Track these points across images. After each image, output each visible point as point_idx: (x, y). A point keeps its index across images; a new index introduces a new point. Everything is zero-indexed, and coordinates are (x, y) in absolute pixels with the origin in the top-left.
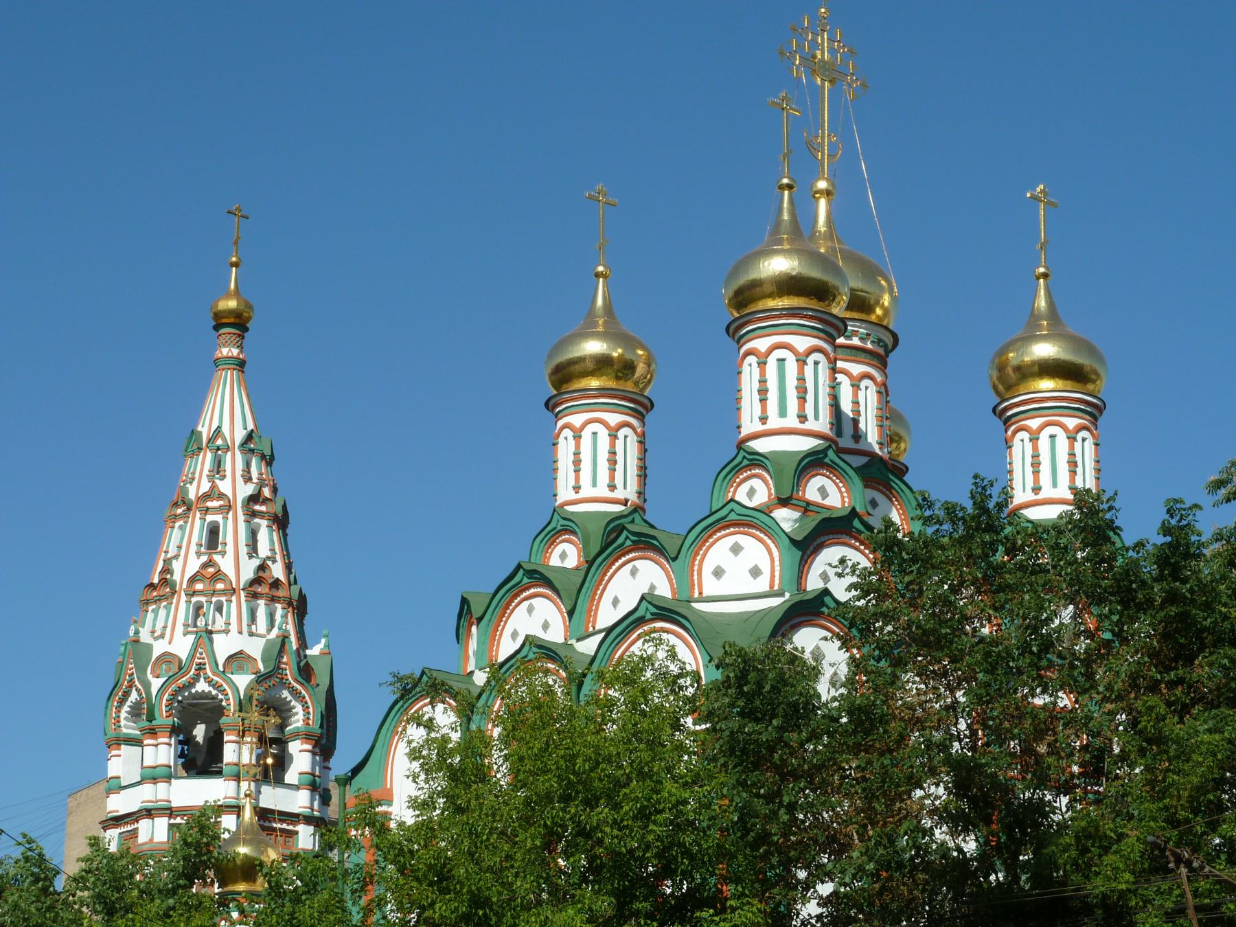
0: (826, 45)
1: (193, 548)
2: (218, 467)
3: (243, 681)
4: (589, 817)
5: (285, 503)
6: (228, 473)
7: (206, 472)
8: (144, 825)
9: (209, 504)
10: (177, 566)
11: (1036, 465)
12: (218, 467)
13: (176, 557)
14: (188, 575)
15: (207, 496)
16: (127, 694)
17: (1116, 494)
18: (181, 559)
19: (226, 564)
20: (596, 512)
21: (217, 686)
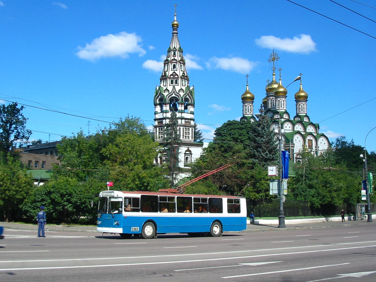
0: (198, 269)
1: (170, 69)
2: (174, 54)
3: (182, 94)
4: (330, 177)
5: (352, 140)
6: (177, 55)
7: (172, 55)
8: (164, 121)
9: (173, 61)
10: (167, 73)
11: (304, 108)
12: (174, 54)
13: (167, 71)
14: (170, 75)
15: (173, 60)
16: (158, 96)
17: (152, 125)
18: (168, 71)
19: (177, 72)
20: (278, 187)
21: (177, 95)
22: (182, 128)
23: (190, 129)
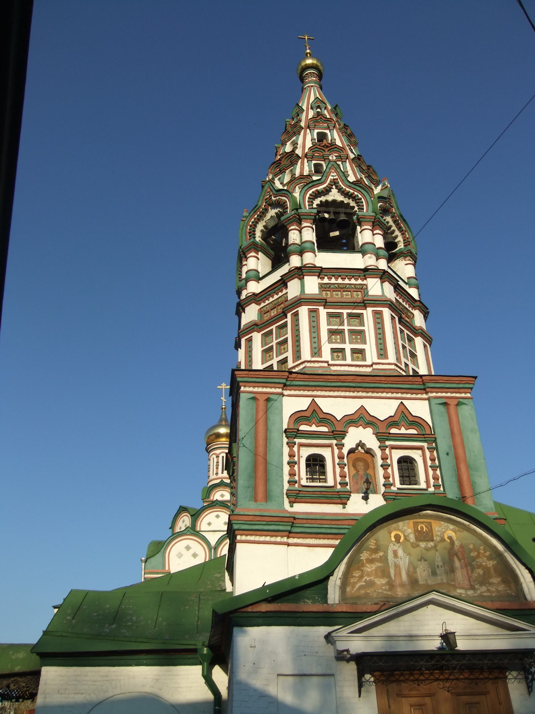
22: (323, 312)
23: (368, 313)
